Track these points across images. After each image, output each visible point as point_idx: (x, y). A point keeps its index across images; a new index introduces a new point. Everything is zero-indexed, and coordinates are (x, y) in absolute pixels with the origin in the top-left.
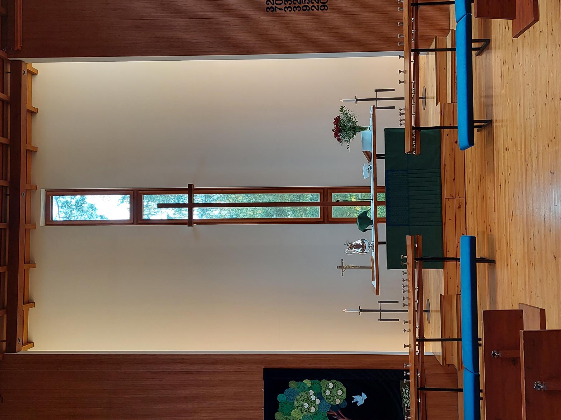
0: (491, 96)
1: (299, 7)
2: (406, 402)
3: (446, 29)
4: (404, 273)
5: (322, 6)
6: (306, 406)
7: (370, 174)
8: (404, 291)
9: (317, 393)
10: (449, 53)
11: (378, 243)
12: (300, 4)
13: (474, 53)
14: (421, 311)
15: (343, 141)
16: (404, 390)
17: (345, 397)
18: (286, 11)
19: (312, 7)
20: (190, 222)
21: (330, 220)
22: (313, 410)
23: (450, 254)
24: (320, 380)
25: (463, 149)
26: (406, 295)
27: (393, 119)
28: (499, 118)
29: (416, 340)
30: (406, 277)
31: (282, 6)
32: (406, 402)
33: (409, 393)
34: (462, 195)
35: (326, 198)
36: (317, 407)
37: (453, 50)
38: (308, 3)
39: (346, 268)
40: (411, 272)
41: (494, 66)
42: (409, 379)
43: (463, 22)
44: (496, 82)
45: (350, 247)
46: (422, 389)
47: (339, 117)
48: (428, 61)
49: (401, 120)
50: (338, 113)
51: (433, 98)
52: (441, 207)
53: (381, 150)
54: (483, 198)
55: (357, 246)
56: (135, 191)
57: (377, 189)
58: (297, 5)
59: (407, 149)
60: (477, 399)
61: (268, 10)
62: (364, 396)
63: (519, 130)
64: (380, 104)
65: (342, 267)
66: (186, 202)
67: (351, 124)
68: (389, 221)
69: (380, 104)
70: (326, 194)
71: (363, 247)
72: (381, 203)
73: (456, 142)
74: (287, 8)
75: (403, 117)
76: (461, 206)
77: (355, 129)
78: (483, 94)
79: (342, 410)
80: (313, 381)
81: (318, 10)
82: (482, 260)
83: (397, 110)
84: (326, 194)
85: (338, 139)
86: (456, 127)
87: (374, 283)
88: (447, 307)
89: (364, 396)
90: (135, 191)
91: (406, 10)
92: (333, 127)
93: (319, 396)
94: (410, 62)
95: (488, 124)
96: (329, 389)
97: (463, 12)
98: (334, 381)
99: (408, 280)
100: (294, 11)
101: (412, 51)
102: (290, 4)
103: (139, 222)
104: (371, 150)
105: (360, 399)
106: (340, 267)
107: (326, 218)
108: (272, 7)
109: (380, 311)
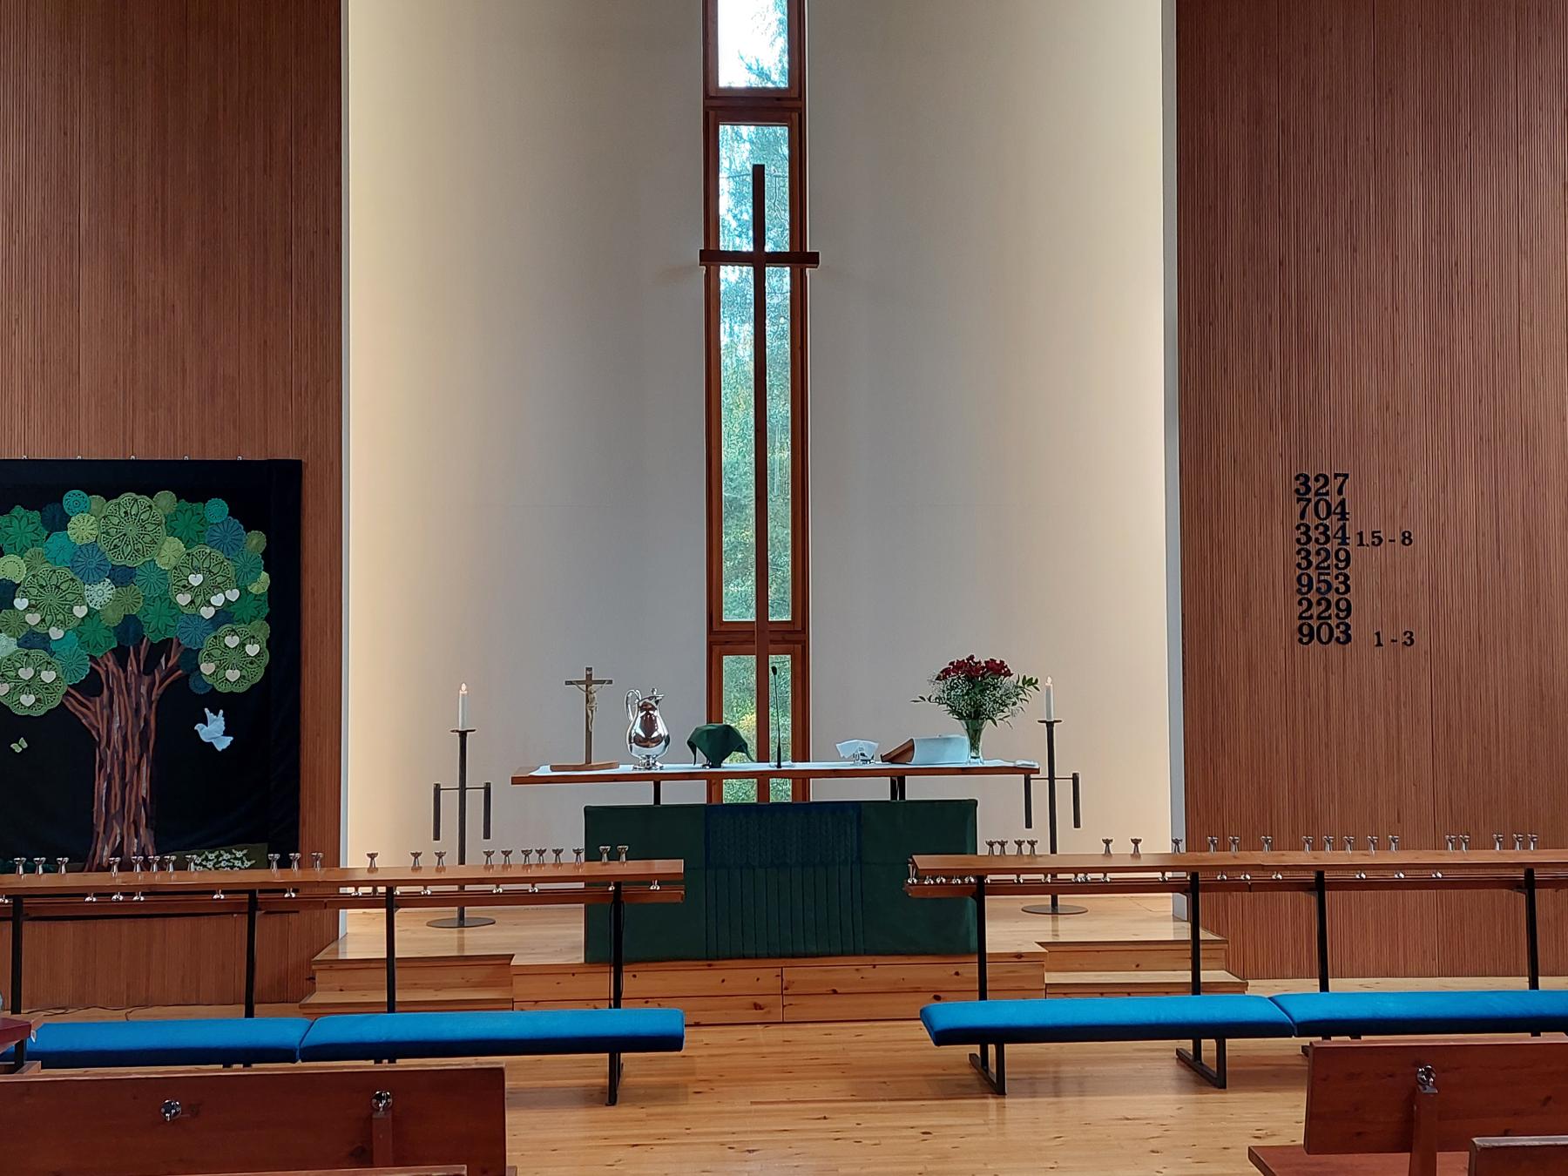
0: (1057, 1093)
1: (1310, 564)
2: (207, 859)
3: (1246, 971)
4: (578, 852)
5: (1311, 628)
6: (196, 580)
7: (845, 762)
8: (527, 853)
9: (232, 609)
10: (1187, 977)
11: (657, 780)
12: (1318, 567)
13: (1188, 1045)
14: (462, 899)
15: (941, 685)
16: (239, 854)
17: (222, 688)
18: (1298, 528)
19: (1309, 601)
20: (713, 257)
21: (716, 649)
22: (183, 599)
23: (632, 983)
24: (267, 619)
25: (924, 1016)
26: (517, 859)
27: (1000, 825)
28: (1010, 1113)
29: (391, 885)
30: (568, 857)
31: (1311, 520)
32: (207, 859)
33: (232, 867)
34: (790, 1014)
35: (779, 637)
36: (193, 611)
37: (1196, 987)
38: (1318, 589)
39: (588, 693)
40: (581, 872)
41: (1142, 1097)
42: (279, 867)
43: (1272, 1014)
44: (1103, 1107)
45: (645, 704)
46: (252, 903)
47: (1008, 674)
48: (1159, 918)
49: (1002, 844)
50: (1018, 672)
51: (1055, 933)
52: (757, 957)
53: (918, 789)
54: (786, 1072)
55: (649, 724)
56: (799, 104)
57: (801, 780)
58: (1314, 560)
59: (923, 861)
60: (226, 1056)
61: (1302, 479)
62: (222, 743)
63: (981, 1166)
64: (1040, 788)
65: (589, 681)
66: (769, 248)
67: (989, 706)
68: (714, 813)
69: (1040, 788)
70: (788, 637)
71: (646, 741)
72: (763, 789)
73: (937, 998)
74: (1306, 533)
75: (1011, 849)
76: (760, 1013)
77: (974, 719)
78: (1068, 1071)
79: (185, 679)
80: (265, 598)
81: (1300, 617)
82: (615, 1070)
83: (1027, 835)
84: (788, 637)
85: (946, 672)
86: (983, 997)
87: (545, 771)
88: (476, 974)
89: (222, 743)
90: (799, 104)
91: (1305, 857)
92: (982, 658)
93: (224, 616)
94: (1162, 869)
95: (993, 1083)
96: (242, 645)
97: (1301, 1013)
98: (266, 659)
99: (558, 864)
100: (1299, 553)
101: (1195, 876)
102: (1317, 540)
103: (711, 113)
104: (917, 760)
105: (214, 731)
106: (589, 676)
107: (723, 639)
108: (1308, 490)
109: (463, 789)
